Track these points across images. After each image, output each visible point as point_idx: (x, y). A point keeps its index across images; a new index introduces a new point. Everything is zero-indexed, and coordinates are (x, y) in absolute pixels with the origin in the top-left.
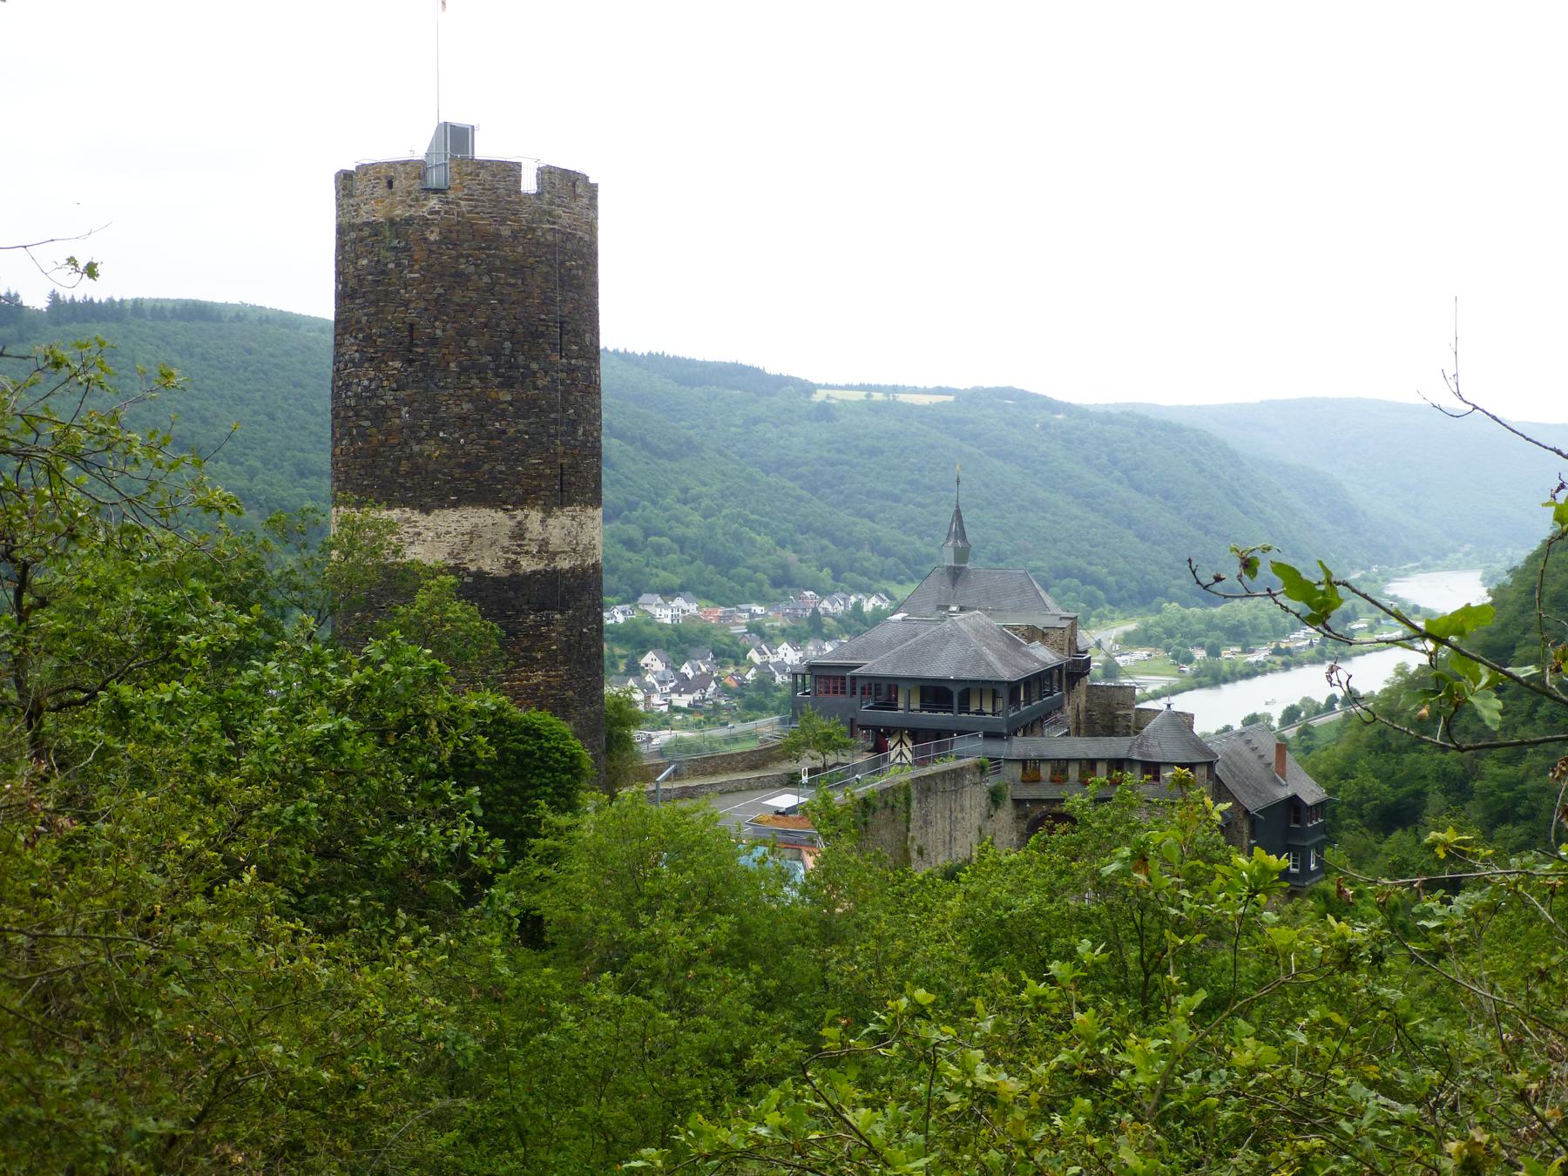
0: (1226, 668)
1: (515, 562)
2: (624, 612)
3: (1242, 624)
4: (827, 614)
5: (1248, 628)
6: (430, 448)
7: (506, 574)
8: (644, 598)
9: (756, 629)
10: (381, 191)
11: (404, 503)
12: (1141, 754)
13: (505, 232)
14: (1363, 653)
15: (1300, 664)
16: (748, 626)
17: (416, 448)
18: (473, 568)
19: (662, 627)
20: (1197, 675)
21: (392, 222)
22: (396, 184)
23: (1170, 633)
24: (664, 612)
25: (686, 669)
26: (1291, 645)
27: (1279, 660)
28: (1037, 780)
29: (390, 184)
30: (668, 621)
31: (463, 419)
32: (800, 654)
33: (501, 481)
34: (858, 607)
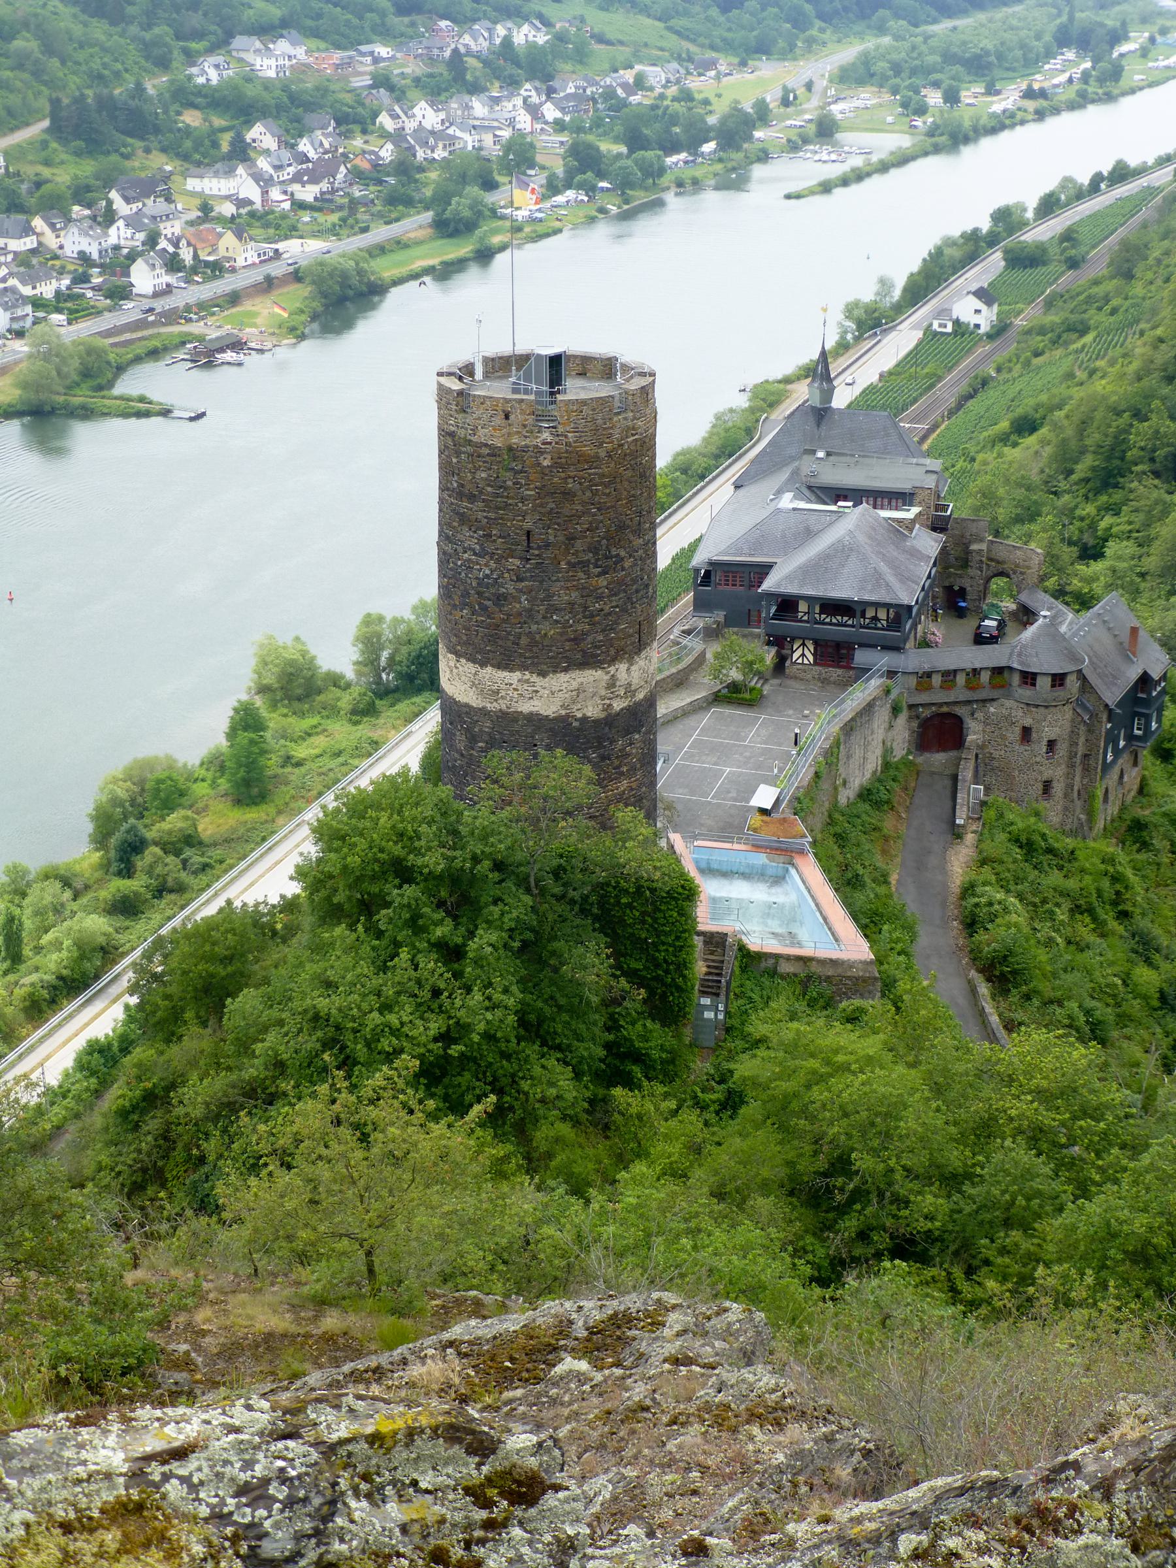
0: (967, 123)
1: (610, 705)
2: (217, 66)
3: (987, 53)
4: (469, 53)
5: (992, 59)
6: (545, 627)
7: (603, 715)
8: (239, 41)
9: (382, 81)
10: (499, 420)
11: (523, 668)
12: (1021, 663)
13: (602, 453)
14: (1133, 91)
15: (1056, 111)
16: (374, 77)
17: (534, 627)
18: (579, 715)
19: (267, 85)
20: (931, 133)
21: (510, 449)
22: (512, 417)
23: (897, 69)
24: (266, 62)
25: (304, 146)
26: (1046, 85)
27: (1031, 105)
28: (930, 688)
29: (507, 417)
30: (272, 74)
31: (572, 604)
32: (442, 115)
33: (599, 647)
34: (507, 42)
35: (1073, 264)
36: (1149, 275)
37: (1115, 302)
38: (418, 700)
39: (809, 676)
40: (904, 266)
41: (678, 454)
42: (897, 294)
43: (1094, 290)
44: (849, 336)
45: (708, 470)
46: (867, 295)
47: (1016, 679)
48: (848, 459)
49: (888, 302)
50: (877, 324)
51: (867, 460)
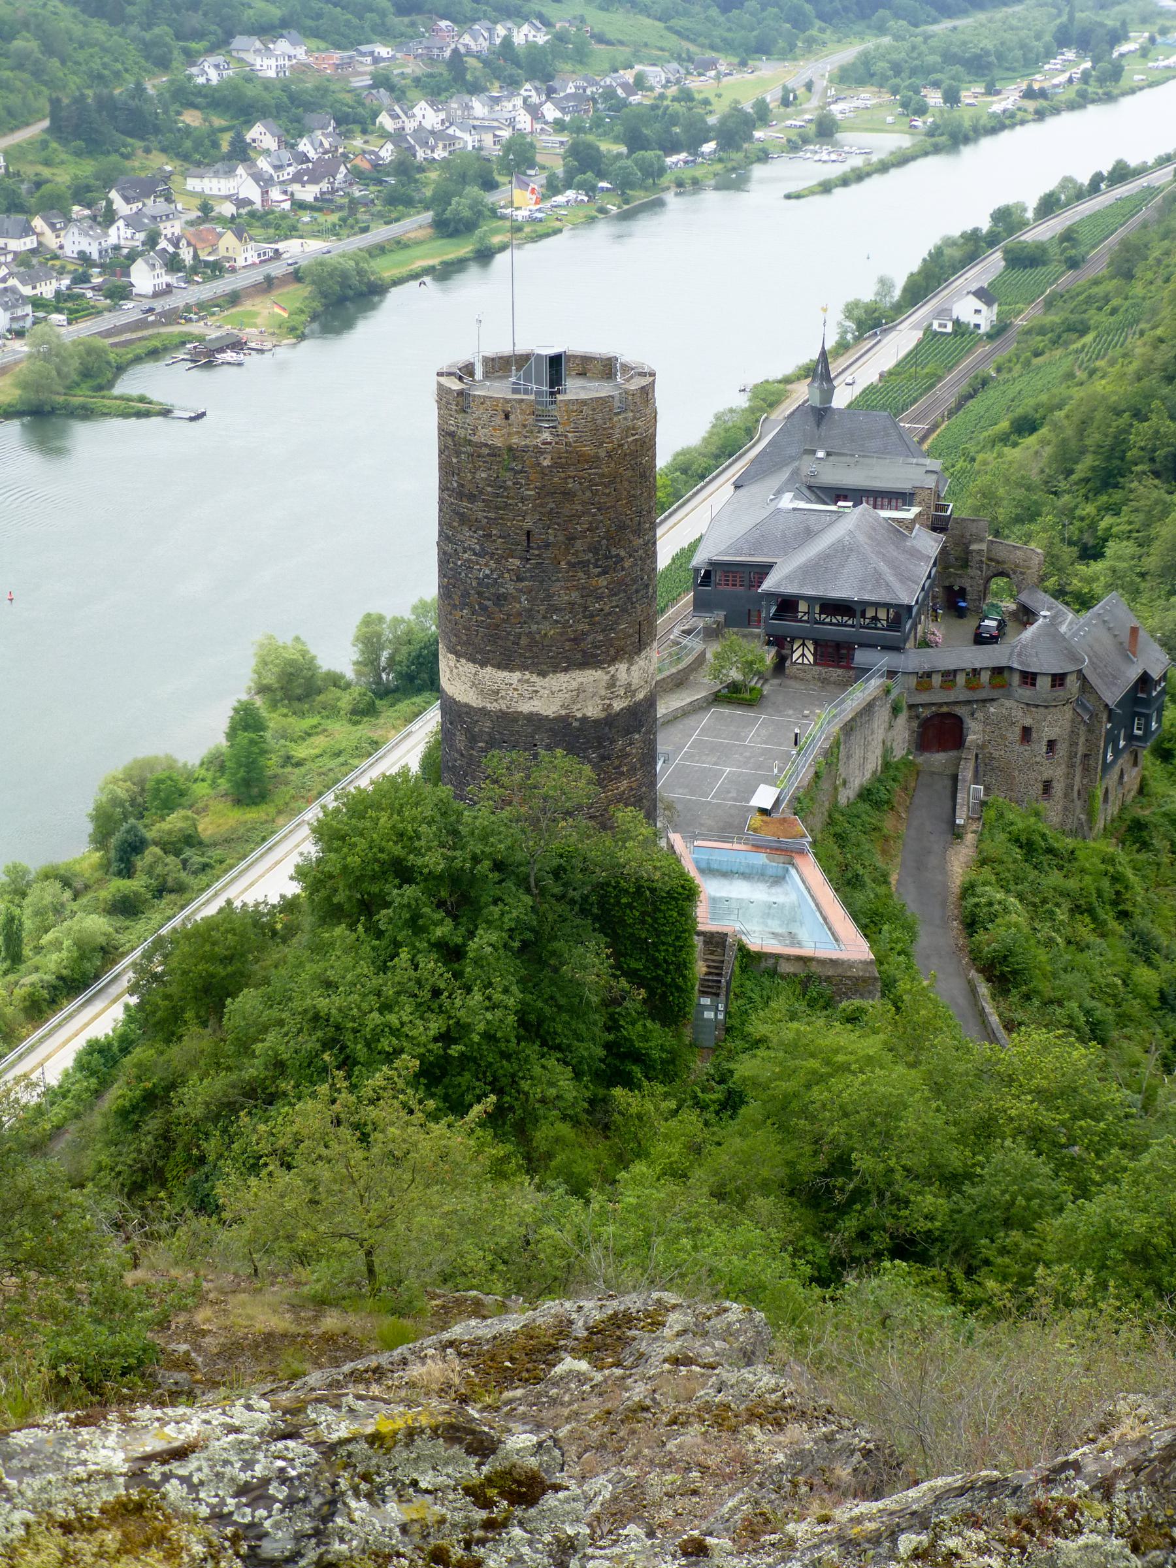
0: (967, 123)
1: (610, 705)
2: (217, 66)
3: (987, 53)
4: (469, 53)
5: (992, 59)
6: (545, 627)
7: (603, 715)
8: (239, 41)
9: (382, 81)
10: (499, 420)
11: (523, 668)
12: (1021, 663)
13: (602, 453)
14: (1133, 91)
15: (1056, 111)
16: (374, 77)
17: (534, 627)
18: (579, 715)
19: (267, 85)
20: (931, 133)
21: (510, 449)
22: (512, 417)
23: (897, 69)
24: (266, 62)
25: (304, 146)
26: (1046, 85)
27: (1031, 105)
28: (930, 688)
29: (507, 417)
30: (272, 74)
31: (572, 604)
32: (442, 115)
33: (599, 647)
34: (507, 42)
35: (1073, 264)
36: (1149, 275)
37: (1115, 302)
38: (418, 700)
39: (809, 676)
40: (904, 266)
41: (678, 454)
42: (897, 294)
43: (1094, 290)
44: (849, 336)
45: (708, 470)
46: (867, 295)
47: (1016, 679)
48: (848, 459)
49: (888, 302)
50: (877, 324)
51: (867, 460)
